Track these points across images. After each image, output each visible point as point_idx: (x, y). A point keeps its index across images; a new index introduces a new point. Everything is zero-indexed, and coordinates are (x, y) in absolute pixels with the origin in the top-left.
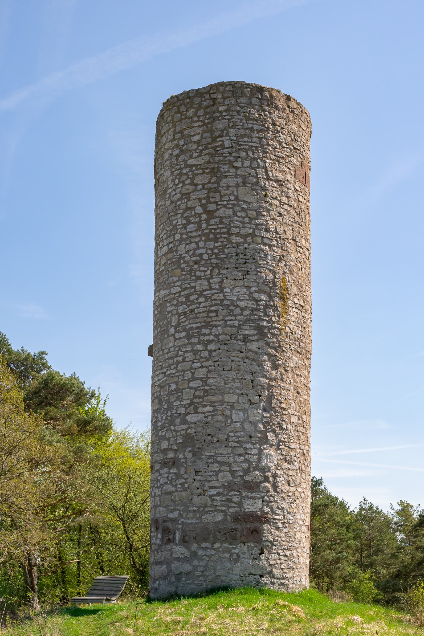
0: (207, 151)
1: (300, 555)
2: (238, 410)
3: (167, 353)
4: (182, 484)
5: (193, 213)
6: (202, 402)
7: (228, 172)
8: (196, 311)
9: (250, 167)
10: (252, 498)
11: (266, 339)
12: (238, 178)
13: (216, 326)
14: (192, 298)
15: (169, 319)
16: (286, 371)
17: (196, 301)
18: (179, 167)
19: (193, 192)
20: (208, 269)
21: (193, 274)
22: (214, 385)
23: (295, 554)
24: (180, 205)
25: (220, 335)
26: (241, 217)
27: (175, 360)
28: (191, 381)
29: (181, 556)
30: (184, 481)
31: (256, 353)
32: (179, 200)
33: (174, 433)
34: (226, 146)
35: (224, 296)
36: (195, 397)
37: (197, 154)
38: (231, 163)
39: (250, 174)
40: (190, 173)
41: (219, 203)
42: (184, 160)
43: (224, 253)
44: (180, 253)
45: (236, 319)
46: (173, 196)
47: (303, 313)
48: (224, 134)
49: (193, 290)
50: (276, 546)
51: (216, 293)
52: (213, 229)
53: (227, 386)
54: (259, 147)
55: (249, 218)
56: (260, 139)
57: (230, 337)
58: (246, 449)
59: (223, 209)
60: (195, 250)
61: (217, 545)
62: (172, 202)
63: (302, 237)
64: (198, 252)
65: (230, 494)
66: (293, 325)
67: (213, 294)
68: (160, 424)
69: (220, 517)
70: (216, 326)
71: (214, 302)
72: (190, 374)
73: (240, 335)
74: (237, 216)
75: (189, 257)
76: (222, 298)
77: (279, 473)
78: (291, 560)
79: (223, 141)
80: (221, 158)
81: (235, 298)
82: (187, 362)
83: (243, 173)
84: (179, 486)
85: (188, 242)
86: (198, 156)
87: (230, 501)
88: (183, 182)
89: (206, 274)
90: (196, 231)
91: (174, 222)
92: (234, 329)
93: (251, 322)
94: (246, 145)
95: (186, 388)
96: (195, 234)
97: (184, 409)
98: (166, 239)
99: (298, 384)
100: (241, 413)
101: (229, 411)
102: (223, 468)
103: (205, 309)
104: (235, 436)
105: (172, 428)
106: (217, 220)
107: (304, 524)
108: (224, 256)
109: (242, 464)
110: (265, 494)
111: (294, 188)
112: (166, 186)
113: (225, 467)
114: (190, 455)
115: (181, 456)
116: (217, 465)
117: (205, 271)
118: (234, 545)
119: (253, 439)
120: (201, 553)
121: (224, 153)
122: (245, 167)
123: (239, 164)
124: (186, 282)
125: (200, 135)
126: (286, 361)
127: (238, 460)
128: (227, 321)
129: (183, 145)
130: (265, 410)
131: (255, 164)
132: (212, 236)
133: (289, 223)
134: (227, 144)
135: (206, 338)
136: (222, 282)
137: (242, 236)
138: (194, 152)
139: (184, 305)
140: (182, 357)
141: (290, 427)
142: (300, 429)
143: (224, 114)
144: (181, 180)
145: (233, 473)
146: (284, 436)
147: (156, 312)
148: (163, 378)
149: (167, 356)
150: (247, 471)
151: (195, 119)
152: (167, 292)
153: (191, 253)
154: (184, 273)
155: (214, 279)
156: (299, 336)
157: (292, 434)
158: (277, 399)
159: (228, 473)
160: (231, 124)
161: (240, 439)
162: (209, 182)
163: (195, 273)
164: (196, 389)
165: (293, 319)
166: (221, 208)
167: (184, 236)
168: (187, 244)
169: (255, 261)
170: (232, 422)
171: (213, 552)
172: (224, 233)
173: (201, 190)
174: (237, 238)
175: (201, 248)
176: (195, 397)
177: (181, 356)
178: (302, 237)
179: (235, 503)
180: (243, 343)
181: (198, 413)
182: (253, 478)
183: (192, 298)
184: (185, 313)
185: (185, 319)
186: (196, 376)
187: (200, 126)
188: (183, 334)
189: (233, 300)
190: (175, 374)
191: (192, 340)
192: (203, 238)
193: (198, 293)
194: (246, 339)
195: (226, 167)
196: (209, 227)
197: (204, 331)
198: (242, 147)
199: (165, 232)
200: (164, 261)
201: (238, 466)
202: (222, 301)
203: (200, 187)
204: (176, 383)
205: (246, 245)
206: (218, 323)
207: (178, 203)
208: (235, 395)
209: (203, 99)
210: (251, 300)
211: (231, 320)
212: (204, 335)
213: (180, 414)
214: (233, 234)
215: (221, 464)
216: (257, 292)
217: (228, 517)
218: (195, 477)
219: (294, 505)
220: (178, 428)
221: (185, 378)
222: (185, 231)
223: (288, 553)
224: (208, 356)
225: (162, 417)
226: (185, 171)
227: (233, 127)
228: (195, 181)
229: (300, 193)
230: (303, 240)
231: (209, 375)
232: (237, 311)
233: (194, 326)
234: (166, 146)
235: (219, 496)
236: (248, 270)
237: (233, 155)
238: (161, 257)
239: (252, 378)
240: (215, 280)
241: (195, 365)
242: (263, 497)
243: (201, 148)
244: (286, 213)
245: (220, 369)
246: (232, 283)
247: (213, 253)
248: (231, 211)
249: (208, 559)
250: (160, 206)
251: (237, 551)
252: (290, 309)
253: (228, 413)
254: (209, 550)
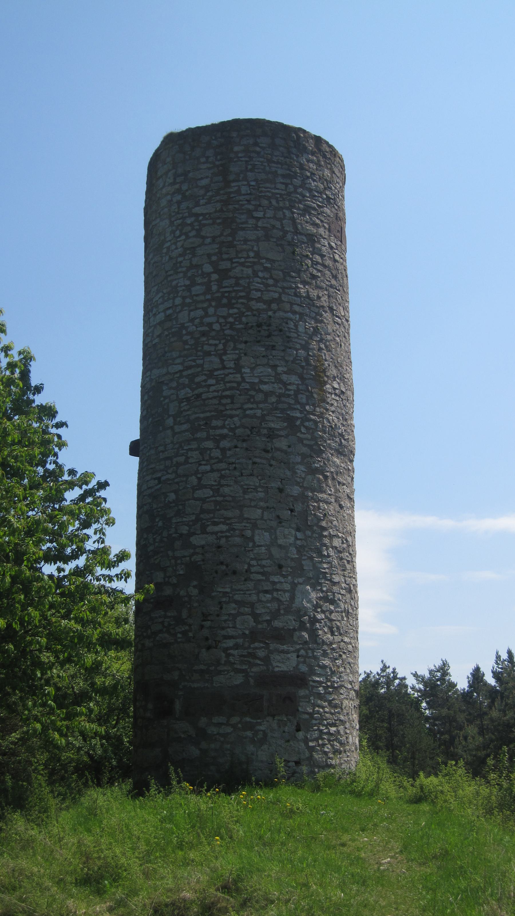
0: (218, 198)
1: (348, 732)
2: (262, 529)
3: (163, 452)
4: (184, 633)
5: (200, 272)
6: (214, 518)
7: (246, 223)
8: (204, 396)
9: (274, 217)
10: (283, 652)
11: (298, 434)
12: (258, 230)
13: (231, 417)
14: (197, 380)
15: (166, 407)
16: (326, 477)
17: (203, 384)
18: (181, 215)
19: (199, 246)
20: (220, 343)
21: (200, 348)
22: (230, 496)
23: (342, 732)
24: (181, 262)
25: (236, 428)
26: (264, 278)
27: (175, 460)
28: (197, 489)
29: (183, 736)
30: (187, 628)
31: (286, 452)
32: (180, 255)
33: (173, 561)
34: (243, 192)
35: (243, 378)
36: (203, 511)
37: (205, 201)
38: (249, 212)
39: (274, 227)
40: (196, 224)
41: (234, 261)
42: (188, 208)
43: (241, 323)
44: (182, 322)
45: (258, 408)
46: (172, 251)
47: (344, 402)
48: (241, 178)
49: (199, 369)
50: (316, 720)
51: (231, 374)
52: (226, 292)
53: (247, 497)
54: (284, 194)
55: (273, 279)
56: (286, 185)
57: (251, 431)
58: (274, 583)
59: (239, 268)
60: (202, 318)
61: (235, 720)
62: (171, 258)
63: (340, 304)
64: (207, 320)
65: (252, 646)
67: (227, 375)
68: (151, 548)
69: (239, 679)
70: (231, 417)
71: (228, 385)
72: (196, 480)
73: (264, 428)
74: (258, 277)
75: (194, 327)
76: (239, 379)
77: (319, 616)
78: (337, 740)
79: (239, 186)
80: (237, 206)
81: (256, 380)
82: (191, 463)
83: (265, 225)
84: (179, 635)
85: (192, 308)
86: (207, 203)
87: (254, 656)
88: (186, 234)
89: (217, 349)
90: (204, 294)
91: (174, 283)
92: (255, 420)
93: (278, 412)
94: (268, 191)
95: (189, 500)
96: (202, 298)
97: (187, 528)
98: (162, 303)
99: (340, 495)
100: (267, 534)
101: (249, 532)
102: (242, 610)
103: (216, 394)
104: (258, 565)
105: (170, 553)
106: (233, 281)
107: (352, 689)
108: (241, 326)
109: (269, 605)
110: (301, 646)
111: (329, 244)
112: (162, 238)
113: (246, 609)
114: (195, 592)
115: (182, 593)
116: (233, 605)
117: (216, 345)
118: (259, 719)
119: (284, 569)
120: (212, 730)
121: (241, 201)
122: (268, 218)
123: (260, 214)
124: (190, 359)
125: (209, 179)
126: (324, 463)
127: (264, 599)
128: (245, 410)
129: (187, 190)
130: (298, 530)
131: (280, 214)
132: (225, 301)
133: (325, 286)
134: (244, 190)
135: (219, 432)
136: (238, 359)
137: (265, 302)
138: (201, 198)
139: (187, 389)
140: (184, 457)
141: (331, 552)
142: (345, 555)
143: (240, 155)
144: (184, 231)
145: (256, 616)
146: (325, 566)
147: (146, 397)
148: (156, 485)
149: (162, 456)
150: (275, 615)
151: (203, 160)
152: (164, 371)
153: (197, 321)
154: (187, 347)
155: (228, 356)
156: (340, 431)
157: (336, 562)
158: (315, 514)
159: (250, 617)
160: (249, 167)
161: (265, 569)
162: (222, 235)
163: (202, 347)
164: (203, 500)
165: (333, 409)
166: (236, 266)
167: (188, 300)
168: (192, 310)
169: (282, 333)
170: (255, 546)
171: (229, 730)
172: (241, 297)
173: (210, 244)
174: (259, 304)
175: (210, 316)
176: (203, 511)
177: (183, 455)
178: (340, 304)
179: (259, 659)
180: (268, 440)
181: (207, 533)
182: (285, 624)
183: (197, 380)
184: (188, 399)
185: (188, 407)
186: (204, 482)
187: (209, 169)
188: (185, 427)
189: (254, 383)
190: (174, 479)
191: (199, 435)
192: (213, 304)
193: (206, 372)
194: (272, 435)
195: (244, 217)
196: (222, 290)
197: (215, 423)
198: (263, 194)
199: (161, 294)
200: (158, 332)
201: (264, 607)
202: (239, 383)
203: (208, 240)
204: (176, 492)
205: (270, 313)
206: (234, 412)
207: (180, 259)
208: (259, 508)
209: (213, 138)
210: (278, 383)
211: (251, 409)
212: (215, 428)
213: (181, 535)
214: (253, 299)
215: (240, 604)
216: (285, 373)
217: (250, 679)
218: (204, 623)
219: (339, 662)
220: (178, 554)
221: (188, 486)
222: (188, 294)
223: (333, 729)
224: (220, 457)
225: (154, 539)
226: (189, 221)
227: (251, 170)
228: (203, 233)
229: (336, 251)
230: (341, 308)
231: (223, 482)
232: (260, 397)
233: (202, 415)
234: (164, 191)
235: (237, 649)
236: (274, 344)
237: (253, 203)
238: (155, 326)
239: (281, 486)
240: (229, 358)
241: (202, 468)
242: (298, 651)
243: (210, 194)
244: (319, 274)
245: (237, 473)
246: (252, 360)
247: (227, 323)
248: (250, 271)
249: (222, 739)
250: (155, 263)
251: (262, 728)
252: (328, 395)
253: (248, 533)
254: (223, 727)
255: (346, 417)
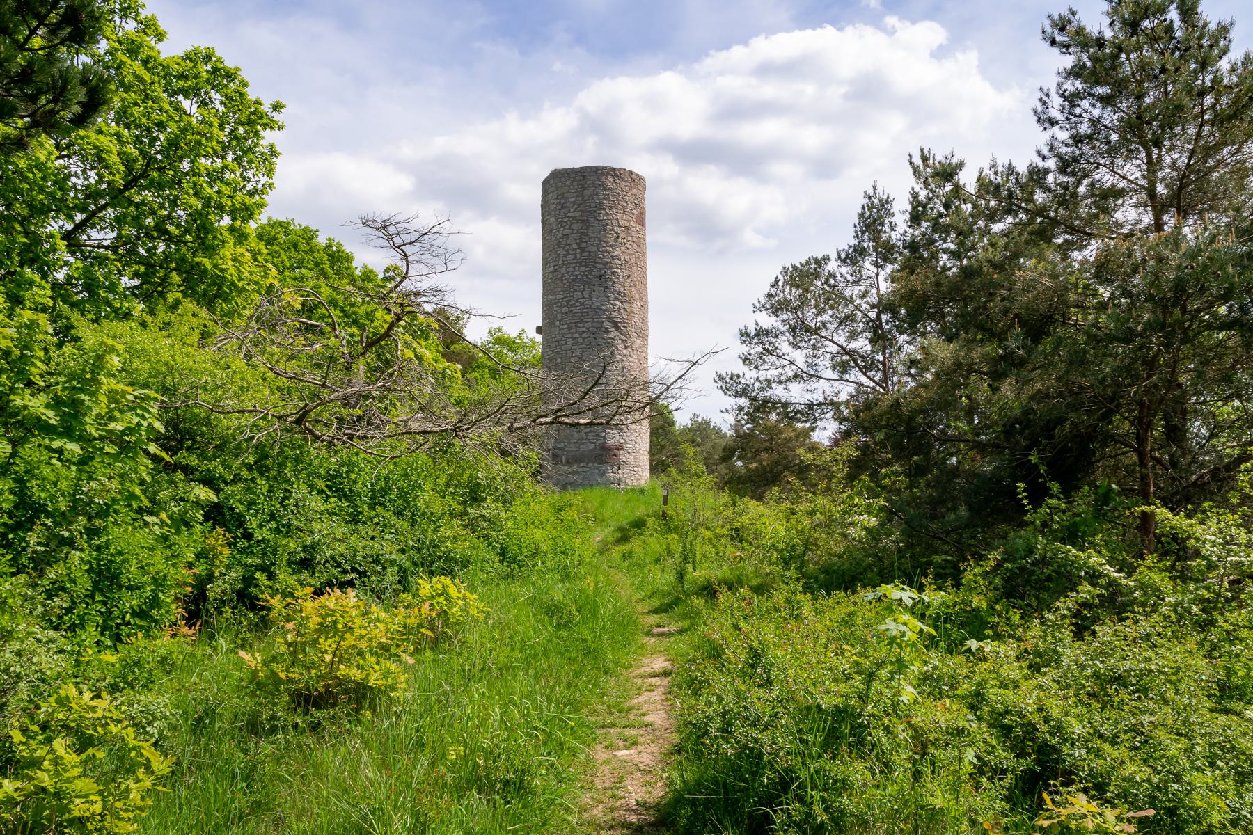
66: (636, 320)
69: (592, 447)
255: (644, 320)
